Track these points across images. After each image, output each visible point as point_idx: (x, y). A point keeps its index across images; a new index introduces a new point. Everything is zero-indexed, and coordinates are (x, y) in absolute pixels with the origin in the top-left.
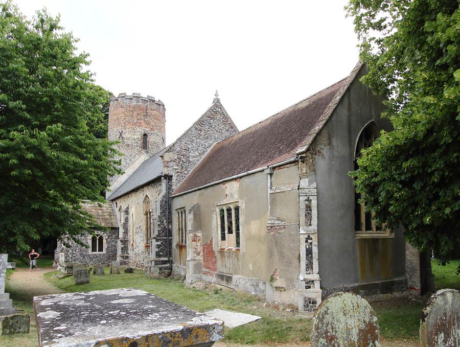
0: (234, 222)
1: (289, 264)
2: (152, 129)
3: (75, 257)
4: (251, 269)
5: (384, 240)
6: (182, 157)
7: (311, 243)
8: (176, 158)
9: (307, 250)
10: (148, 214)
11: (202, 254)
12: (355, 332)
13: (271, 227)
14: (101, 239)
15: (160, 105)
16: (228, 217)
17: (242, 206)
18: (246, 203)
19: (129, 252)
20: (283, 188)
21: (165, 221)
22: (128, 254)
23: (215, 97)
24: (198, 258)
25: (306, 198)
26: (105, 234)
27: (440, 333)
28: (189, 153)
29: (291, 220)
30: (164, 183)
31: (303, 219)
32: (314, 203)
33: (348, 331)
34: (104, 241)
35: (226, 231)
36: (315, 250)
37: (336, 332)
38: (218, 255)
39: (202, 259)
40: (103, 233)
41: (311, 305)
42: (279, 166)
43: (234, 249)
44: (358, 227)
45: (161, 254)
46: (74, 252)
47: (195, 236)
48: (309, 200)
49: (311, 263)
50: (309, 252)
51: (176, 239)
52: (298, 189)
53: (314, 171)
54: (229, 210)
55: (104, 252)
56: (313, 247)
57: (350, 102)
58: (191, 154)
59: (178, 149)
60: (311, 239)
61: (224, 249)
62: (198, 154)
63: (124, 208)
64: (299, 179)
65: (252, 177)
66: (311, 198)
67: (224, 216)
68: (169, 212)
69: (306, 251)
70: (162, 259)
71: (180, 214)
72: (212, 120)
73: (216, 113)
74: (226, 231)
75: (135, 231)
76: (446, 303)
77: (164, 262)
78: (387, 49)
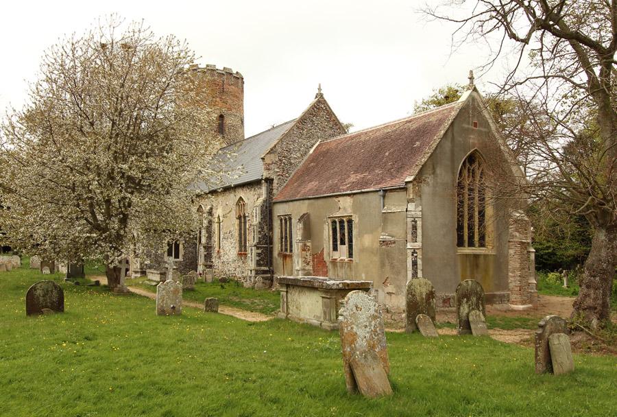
0: (346, 234)
1: (398, 273)
5: (486, 256)
7: (416, 256)
8: (277, 159)
9: (413, 262)
10: (242, 218)
11: (311, 263)
12: (424, 294)
13: (383, 242)
15: (239, 79)
16: (340, 229)
17: (356, 219)
18: (359, 217)
19: (214, 260)
20: (394, 209)
22: (212, 262)
23: (317, 92)
24: (307, 268)
25: (412, 219)
30: (263, 190)
31: (409, 236)
32: (419, 223)
33: (421, 293)
34: (181, 246)
35: (339, 243)
38: (330, 266)
42: (391, 190)
43: (346, 260)
44: (460, 243)
47: (305, 245)
50: (415, 264)
51: (277, 247)
52: (407, 211)
53: (420, 196)
54: (342, 222)
55: (181, 259)
57: (453, 135)
59: (280, 150)
60: (416, 253)
61: (336, 260)
62: (299, 155)
63: (206, 209)
64: (406, 202)
65: (365, 196)
66: (416, 219)
67: (336, 227)
68: (270, 219)
70: (263, 268)
71: (283, 221)
73: (320, 110)
74: (339, 243)
76: (468, 285)
77: (265, 272)
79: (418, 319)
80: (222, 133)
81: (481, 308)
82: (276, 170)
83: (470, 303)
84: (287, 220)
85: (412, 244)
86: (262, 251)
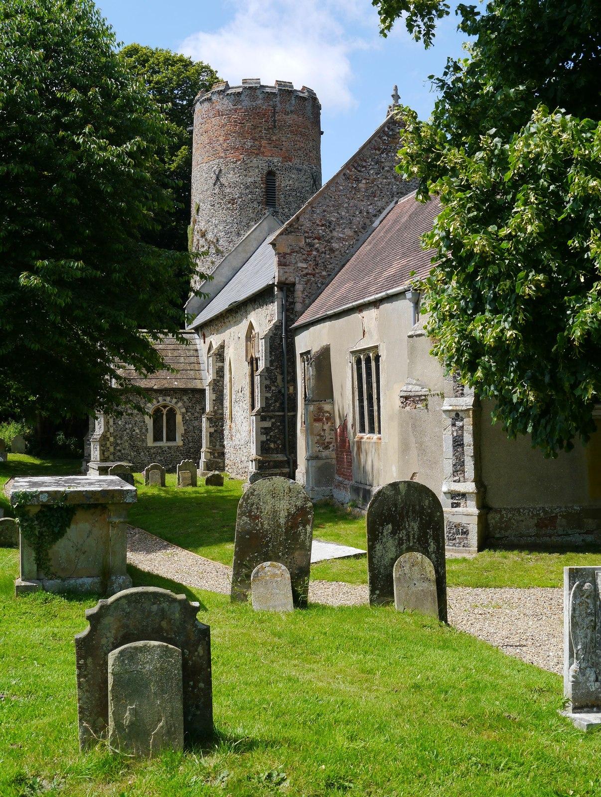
2: (287, 159)
3: (120, 451)
6: (316, 241)
9: (454, 441)
10: (253, 362)
12: (283, 514)
14: (172, 414)
17: (382, 352)
21: (279, 377)
24: (325, 453)
26: (180, 404)
27: (387, 524)
28: (331, 231)
29: (436, 385)
33: (275, 512)
34: (179, 418)
36: (468, 439)
37: (261, 512)
39: (334, 456)
40: (174, 400)
41: (460, 536)
45: (272, 446)
46: (119, 441)
49: (462, 464)
55: (179, 442)
56: (465, 434)
58: (335, 234)
69: (454, 441)
71: (363, 363)
72: (384, 155)
75: (234, 397)
78: (415, 169)
79: (257, 573)
80: (274, 206)
81: (432, 547)
82: (300, 265)
83: (402, 534)
84: (322, 361)
85: (454, 401)
86: (273, 424)
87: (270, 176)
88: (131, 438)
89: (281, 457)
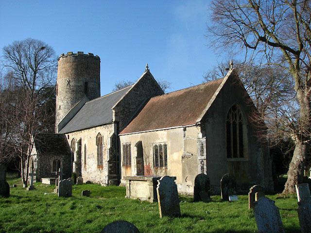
4: (299, 201)
21: (115, 151)
34: (61, 163)
48: (202, 144)
77: (114, 178)
84: (127, 147)
87: (86, 84)
88: (46, 170)
89: (115, 175)
